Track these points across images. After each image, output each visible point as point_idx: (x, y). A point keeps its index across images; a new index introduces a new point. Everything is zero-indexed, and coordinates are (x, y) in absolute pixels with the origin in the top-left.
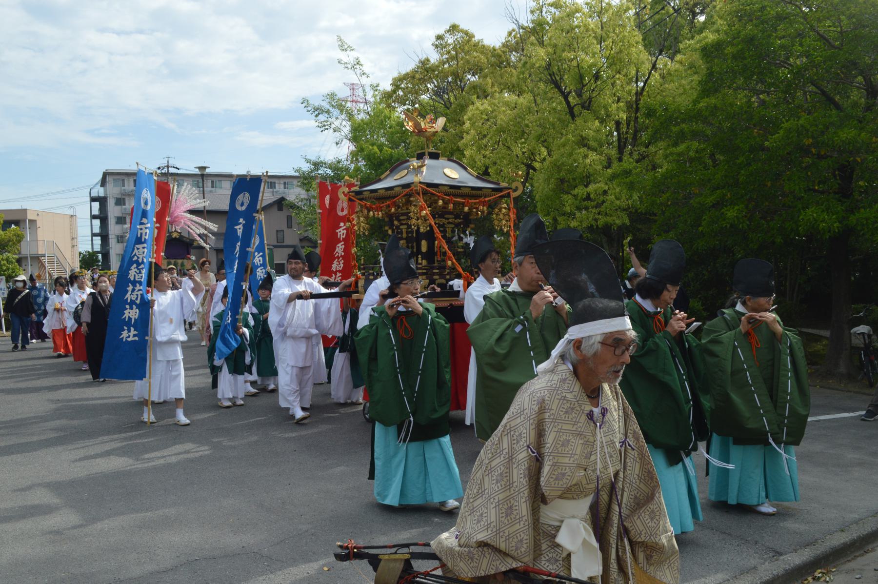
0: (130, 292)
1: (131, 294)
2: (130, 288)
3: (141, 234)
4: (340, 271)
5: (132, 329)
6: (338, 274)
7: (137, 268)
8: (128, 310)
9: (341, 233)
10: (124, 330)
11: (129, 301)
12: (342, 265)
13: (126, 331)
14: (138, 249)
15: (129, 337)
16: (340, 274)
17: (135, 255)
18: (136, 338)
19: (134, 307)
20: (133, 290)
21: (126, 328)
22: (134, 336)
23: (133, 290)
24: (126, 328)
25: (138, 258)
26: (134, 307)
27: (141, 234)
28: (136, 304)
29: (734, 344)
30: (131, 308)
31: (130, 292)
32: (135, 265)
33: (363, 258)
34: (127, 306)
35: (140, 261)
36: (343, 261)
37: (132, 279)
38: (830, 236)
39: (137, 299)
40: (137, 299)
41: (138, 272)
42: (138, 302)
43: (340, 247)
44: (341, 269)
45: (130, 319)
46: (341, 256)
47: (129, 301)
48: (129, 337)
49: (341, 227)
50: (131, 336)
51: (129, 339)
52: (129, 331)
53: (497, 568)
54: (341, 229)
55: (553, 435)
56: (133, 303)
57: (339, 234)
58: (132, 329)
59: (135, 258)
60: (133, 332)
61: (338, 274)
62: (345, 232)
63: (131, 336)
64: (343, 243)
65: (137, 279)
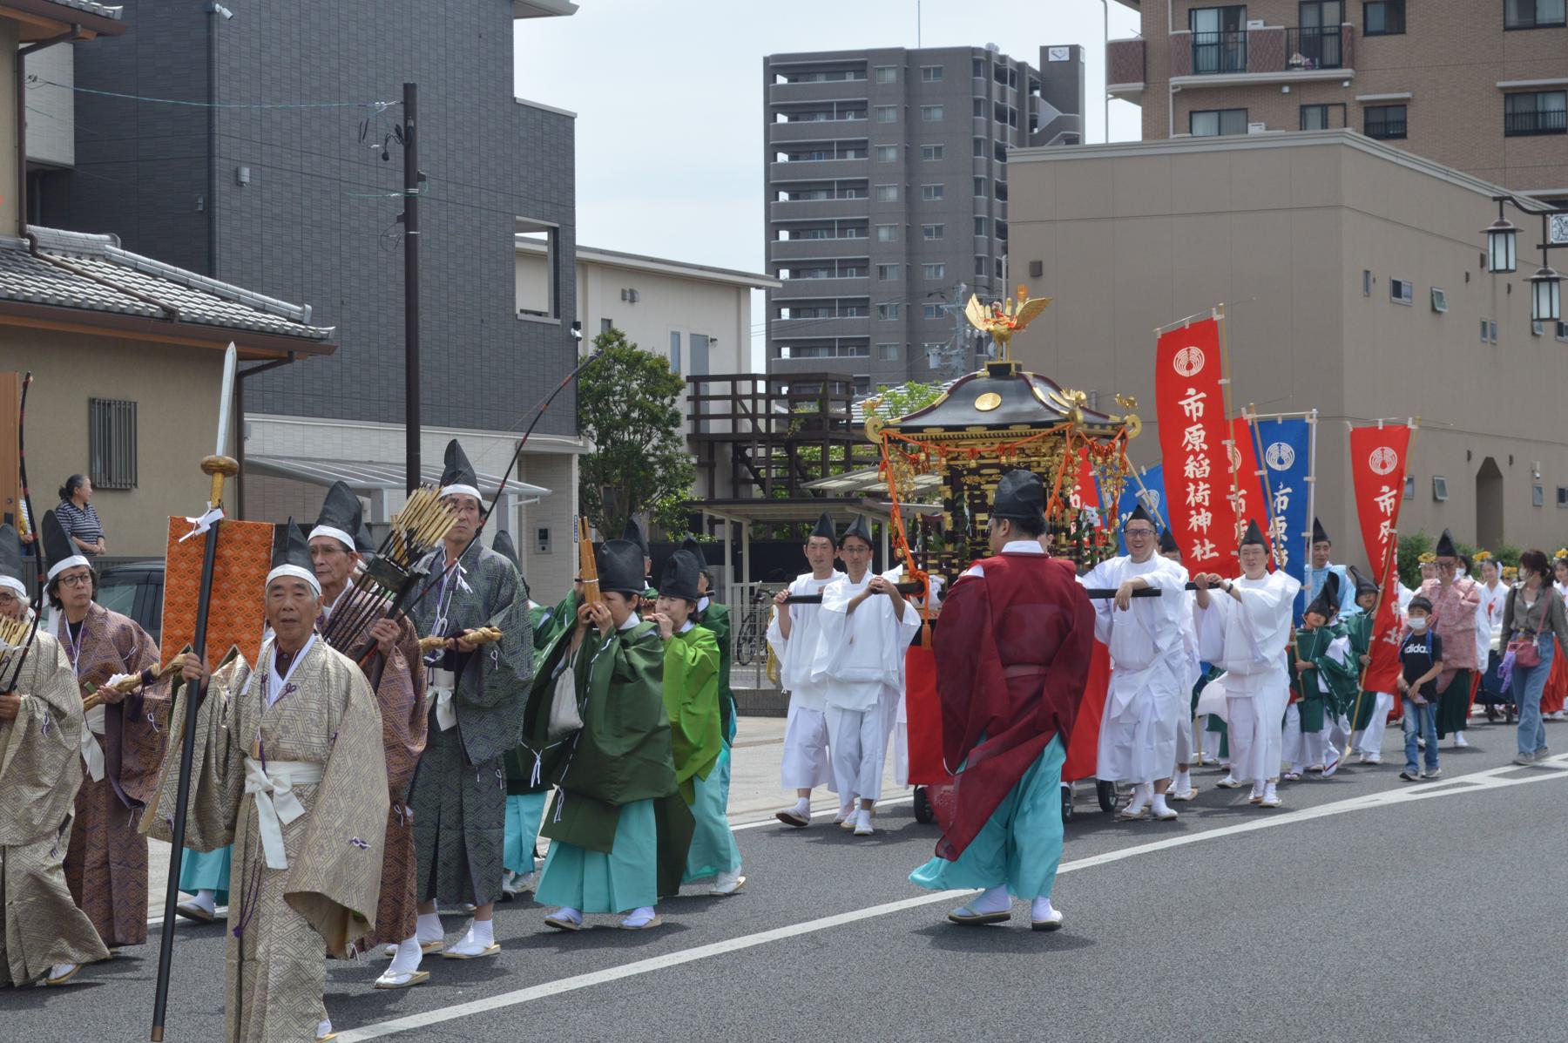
0: (1192, 494)
1: (1195, 496)
2: (1192, 487)
3: (1191, 411)
4: (1204, 480)
5: (1206, 541)
6: (1202, 486)
7: (1195, 460)
8: (1195, 517)
9: (1193, 407)
10: (1195, 545)
11: (1193, 505)
12: (1208, 469)
13: (1199, 546)
14: (1191, 433)
15: (1204, 553)
16: (1207, 486)
17: (1188, 442)
18: (1216, 554)
19: (1203, 510)
20: (1196, 491)
21: (1196, 541)
22: (1212, 550)
23: (1196, 491)
24: (1196, 541)
25: (1194, 445)
26: (1203, 510)
27: (1191, 411)
28: (1204, 507)
29: (475, 905)
30: (1199, 513)
31: (1192, 494)
32: (1192, 457)
33: (82, 560)
34: (1193, 512)
35: (1198, 449)
36: (1207, 461)
37: (1192, 476)
38: (801, 424)
39: (1204, 500)
40: (1204, 500)
41: (1198, 465)
42: (1207, 503)
43: (1196, 434)
44: (1206, 475)
45: (1200, 528)
46: (1202, 451)
47: (1193, 505)
48: (1204, 553)
49: (1190, 396)
50: (1208, 552)
51: (1205, 557)
52: (1203, 545)
53: (313, 887)
54: (1191, 400)
55: (177, 756)
56: (1198, 506)
57: (1187, 410)
58: (1206, 541)
59: (1190, 447)
60: (1209, 546)
61: (1202, 486)
62: (1201, 405)
63: (1208, 552)
64: (1200, 426)
65: (1198, 476)
